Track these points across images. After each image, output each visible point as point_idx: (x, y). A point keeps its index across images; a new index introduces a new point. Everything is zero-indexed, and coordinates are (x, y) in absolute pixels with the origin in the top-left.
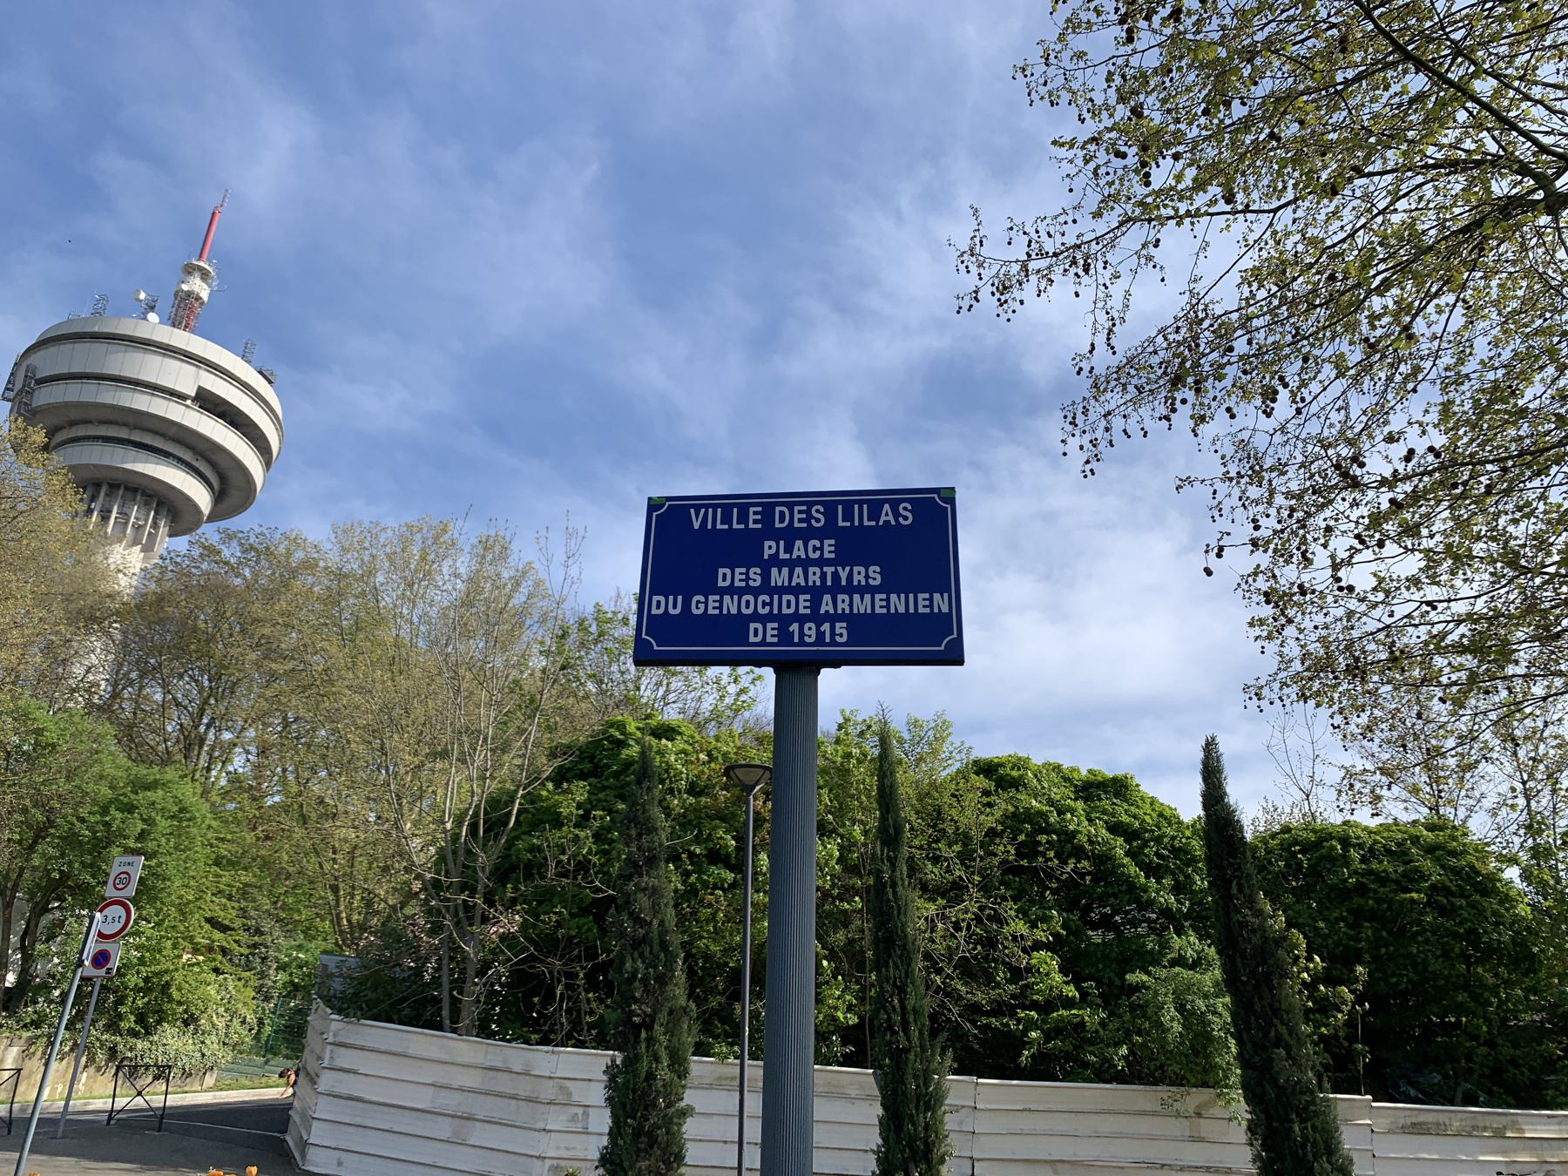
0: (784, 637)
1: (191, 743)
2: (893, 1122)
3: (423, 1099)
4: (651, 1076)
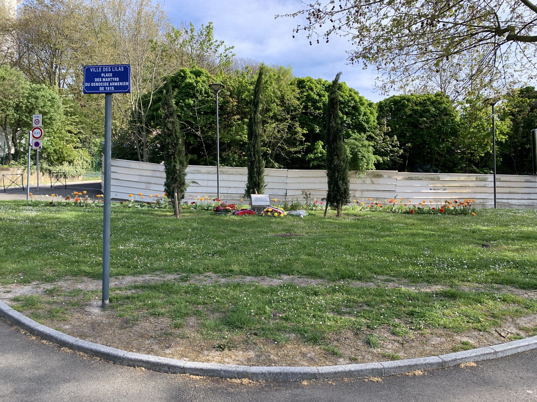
0: (105, 89)
1: (51, 75)
3: (136, 179)
4: (175, 166)
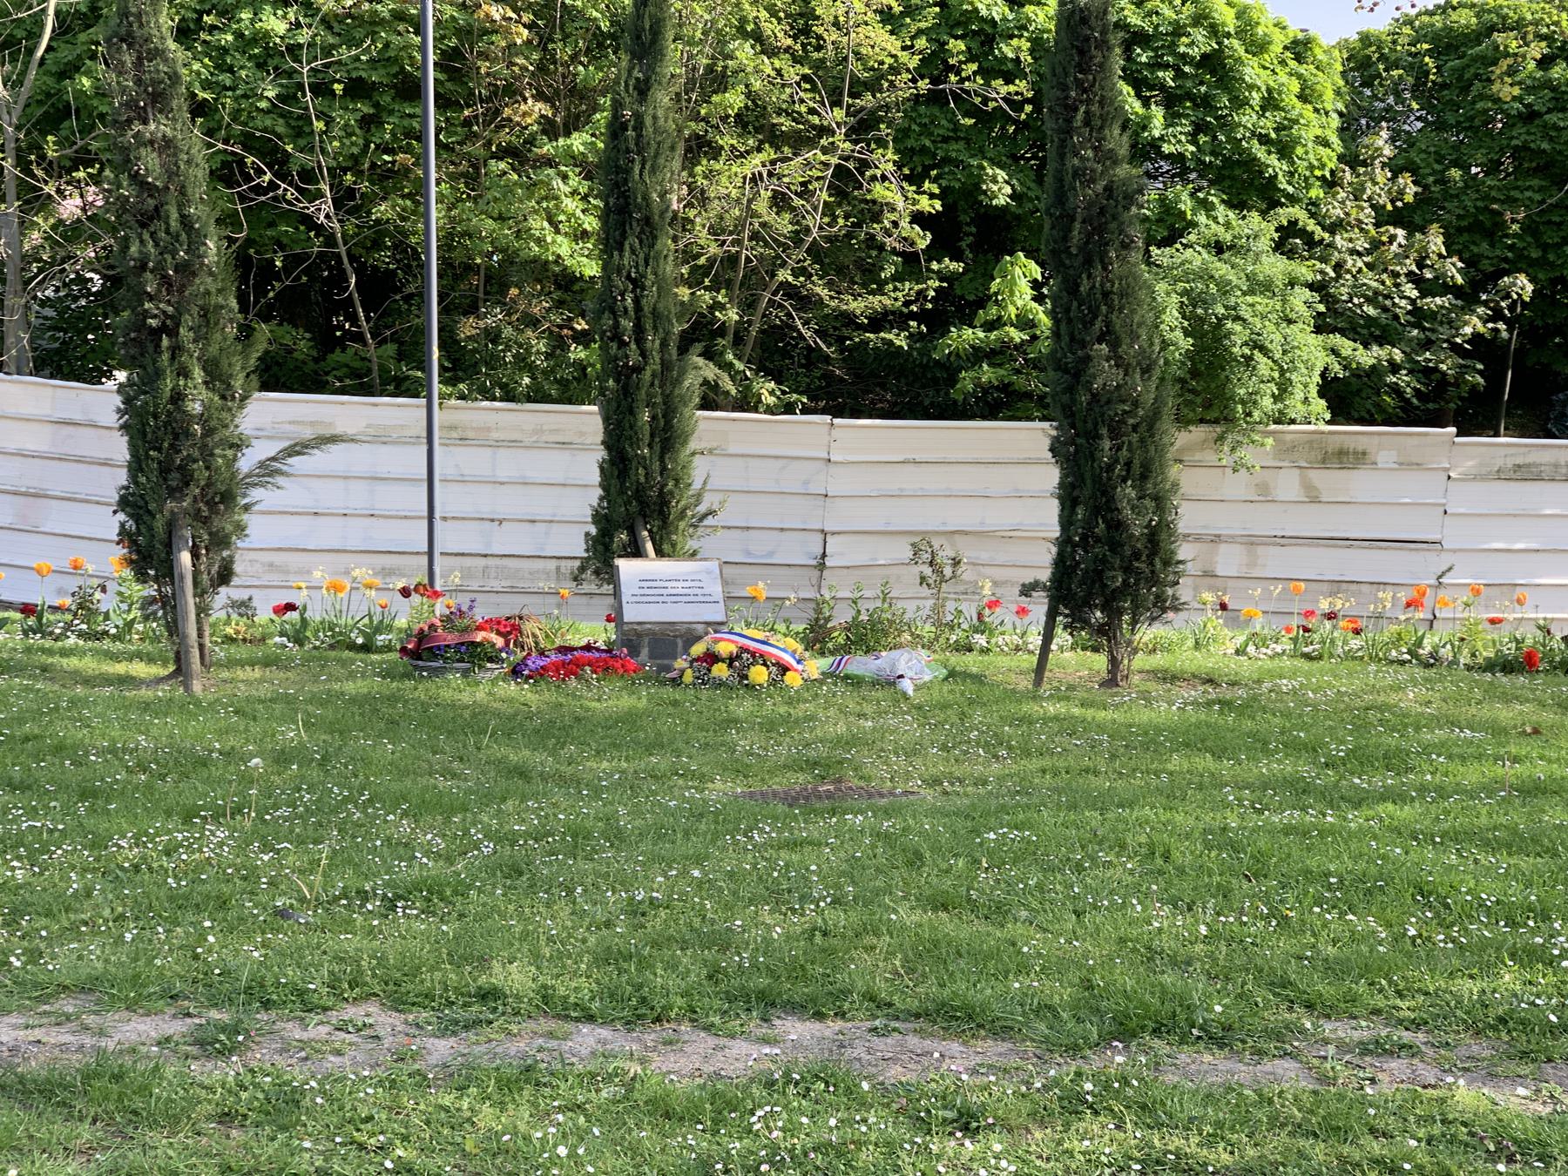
2: (617, 466)
4: (178, 397)
